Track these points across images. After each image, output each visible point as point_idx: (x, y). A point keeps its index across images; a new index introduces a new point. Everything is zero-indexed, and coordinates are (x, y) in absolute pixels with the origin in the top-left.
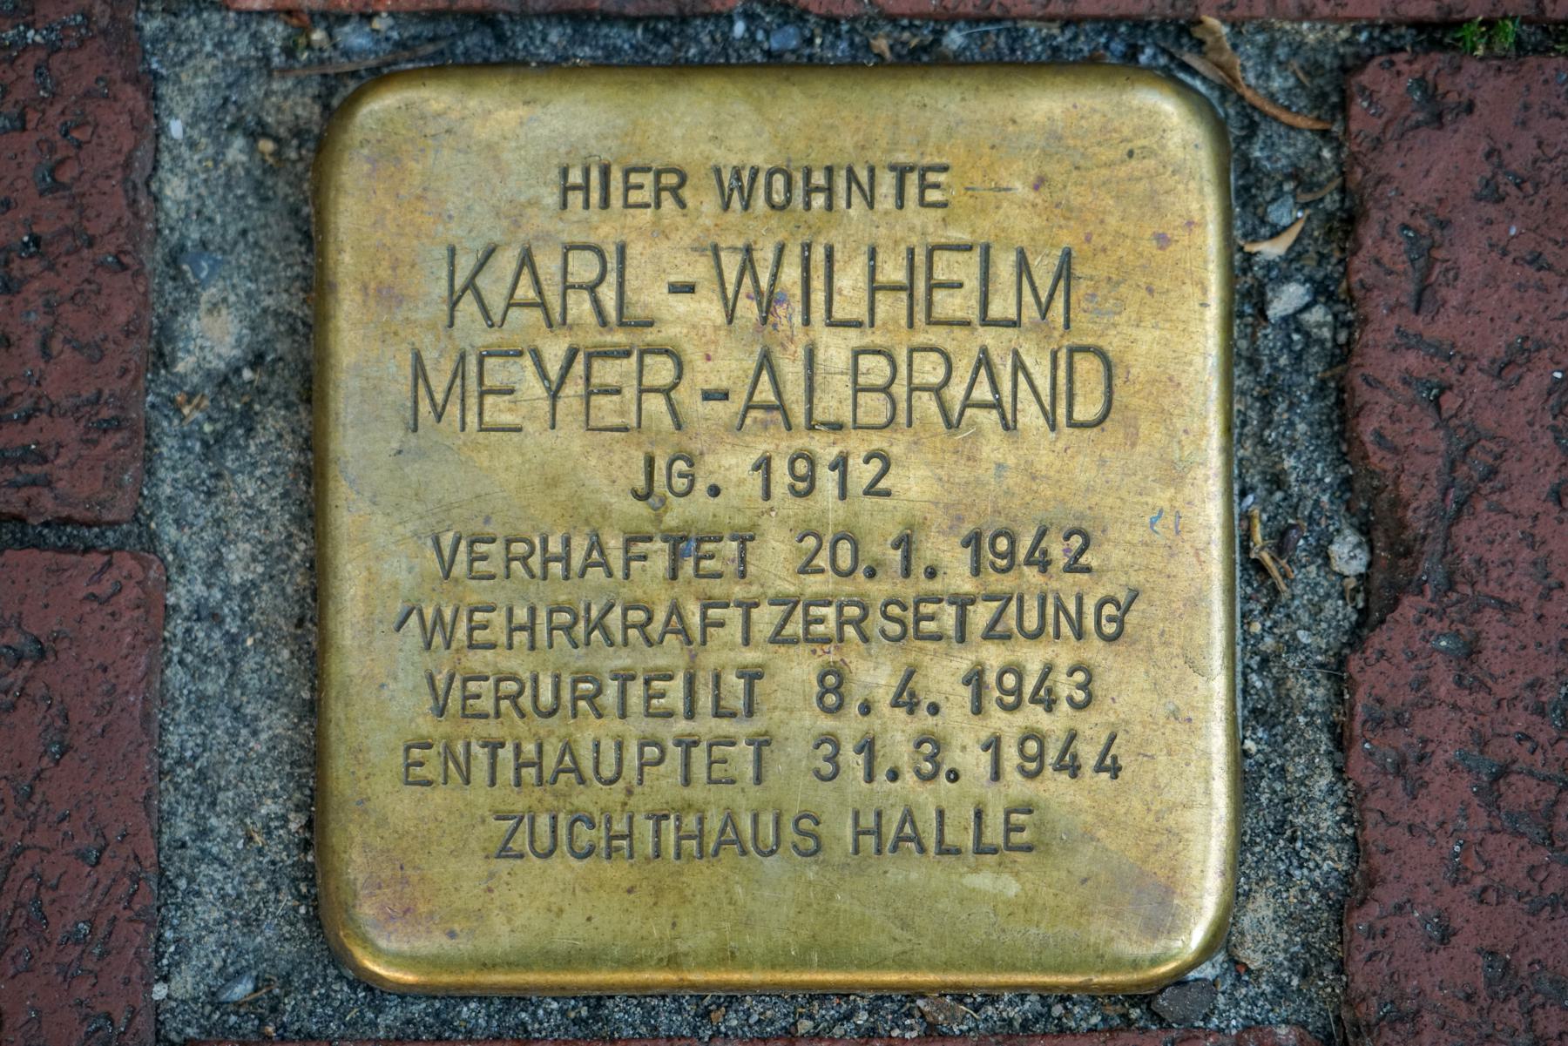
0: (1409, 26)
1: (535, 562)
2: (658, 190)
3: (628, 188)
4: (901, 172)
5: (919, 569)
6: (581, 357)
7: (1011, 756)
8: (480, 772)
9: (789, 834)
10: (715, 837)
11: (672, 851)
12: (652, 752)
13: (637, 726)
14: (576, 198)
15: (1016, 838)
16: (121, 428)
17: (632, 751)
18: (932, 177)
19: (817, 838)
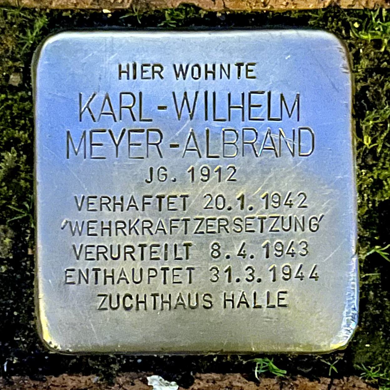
0: (356, 85)
1: (111, 205)
2: (154, 72)
3: (143, 71)
4: (239, 65)
5: (247, 208)
6: (126, 132)
7: (273, 252)
8: (137, 255)
9: (202, 303)
10: (175, 302)
11: (160, 307)
12: (153, 273)
13: (138, 265)
14: (124, 75)
15: (282, 302)
16: (370, 229)
17: (145, 274)
18: (250, 67)
19: (211, 302)
